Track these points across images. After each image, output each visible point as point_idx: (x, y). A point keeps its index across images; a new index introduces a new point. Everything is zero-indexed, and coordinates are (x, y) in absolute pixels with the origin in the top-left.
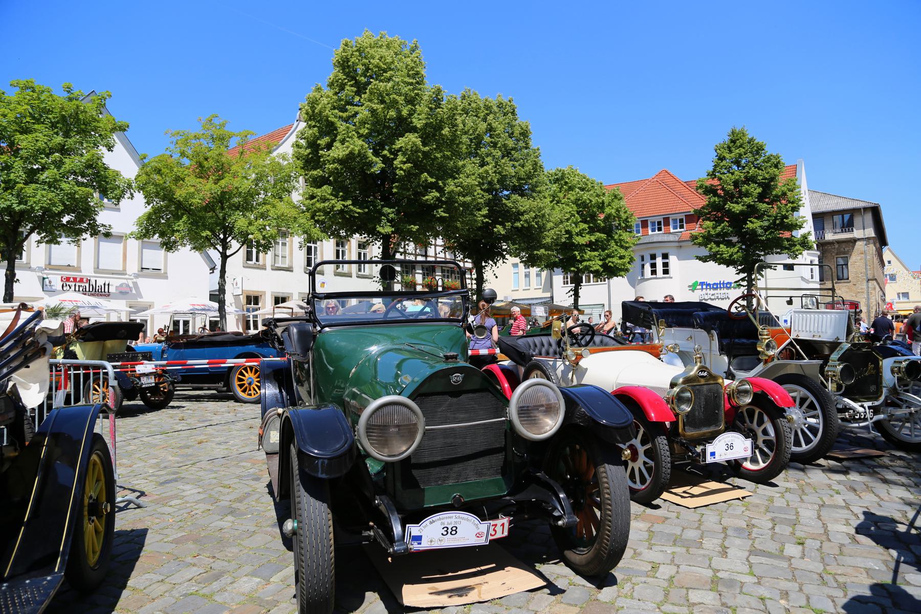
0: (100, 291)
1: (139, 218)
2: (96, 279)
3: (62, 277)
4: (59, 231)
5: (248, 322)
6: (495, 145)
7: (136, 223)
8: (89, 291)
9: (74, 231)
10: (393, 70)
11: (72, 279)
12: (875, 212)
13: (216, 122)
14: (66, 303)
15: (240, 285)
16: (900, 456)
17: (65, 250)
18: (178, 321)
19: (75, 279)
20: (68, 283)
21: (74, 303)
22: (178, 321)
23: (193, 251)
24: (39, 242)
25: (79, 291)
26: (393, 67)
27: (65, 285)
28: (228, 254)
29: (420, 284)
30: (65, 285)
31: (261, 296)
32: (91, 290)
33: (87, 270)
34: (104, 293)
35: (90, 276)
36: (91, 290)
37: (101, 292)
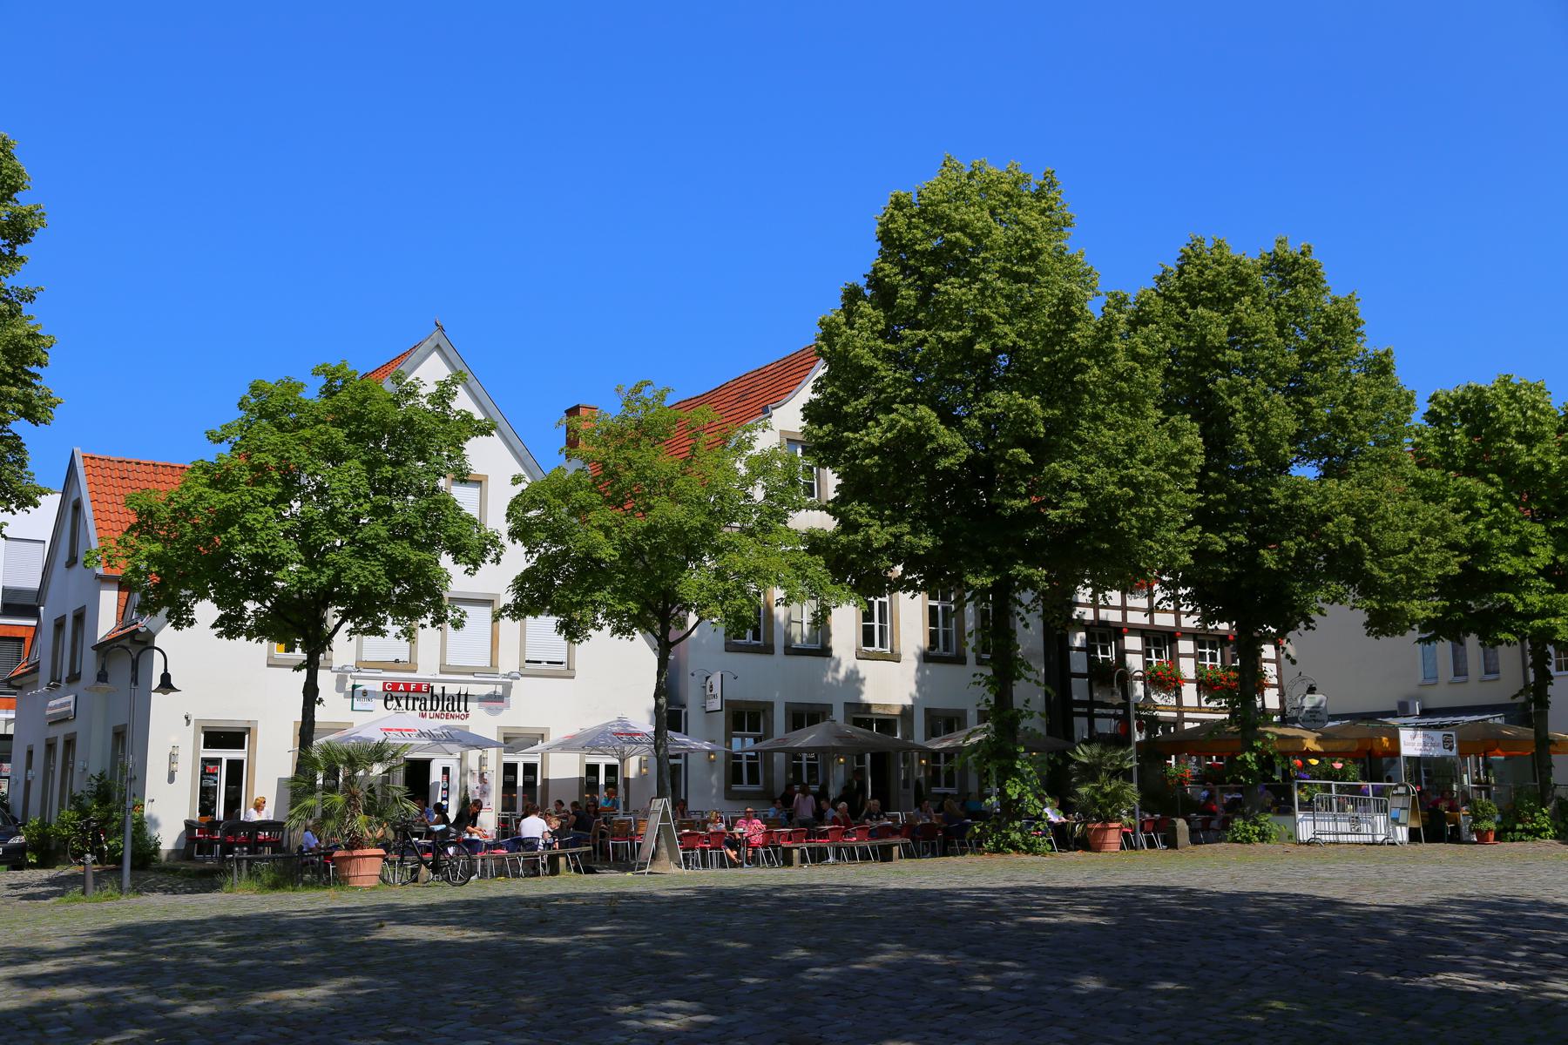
0: (450, 709)
1: (517, 578)
2: (443, 685)
3: (385, 684)
4: (384, 612)
5: (737, 767)
6: (1249, 369)
7: (511, 588)
8: (432, 709)
9: (407, 610)
10: (986, 249)
11: (401, 687)
12: (352, 709)
13: (648, 393)
14: (392, 735)
15: (717, 690)
16: (1316, 1025)
17: (388, 645)
18: (515, 766)
19: (407, 686)
20: (394, 694)
21: (406, 733)
22: (515, 766)
23: (617, 636)
24: (351, 632)
25: (414, 709)
26: (986, 242)
27: (389, 697)
28: (671, 639)
29: (1190, 681)
30: (389, 697)
31: (764, 711)
32: (435, 708)
33: (427, 671)
34: (457, 712)
35: (435, 681)
36: (435, 708)
37: (453, 710)
